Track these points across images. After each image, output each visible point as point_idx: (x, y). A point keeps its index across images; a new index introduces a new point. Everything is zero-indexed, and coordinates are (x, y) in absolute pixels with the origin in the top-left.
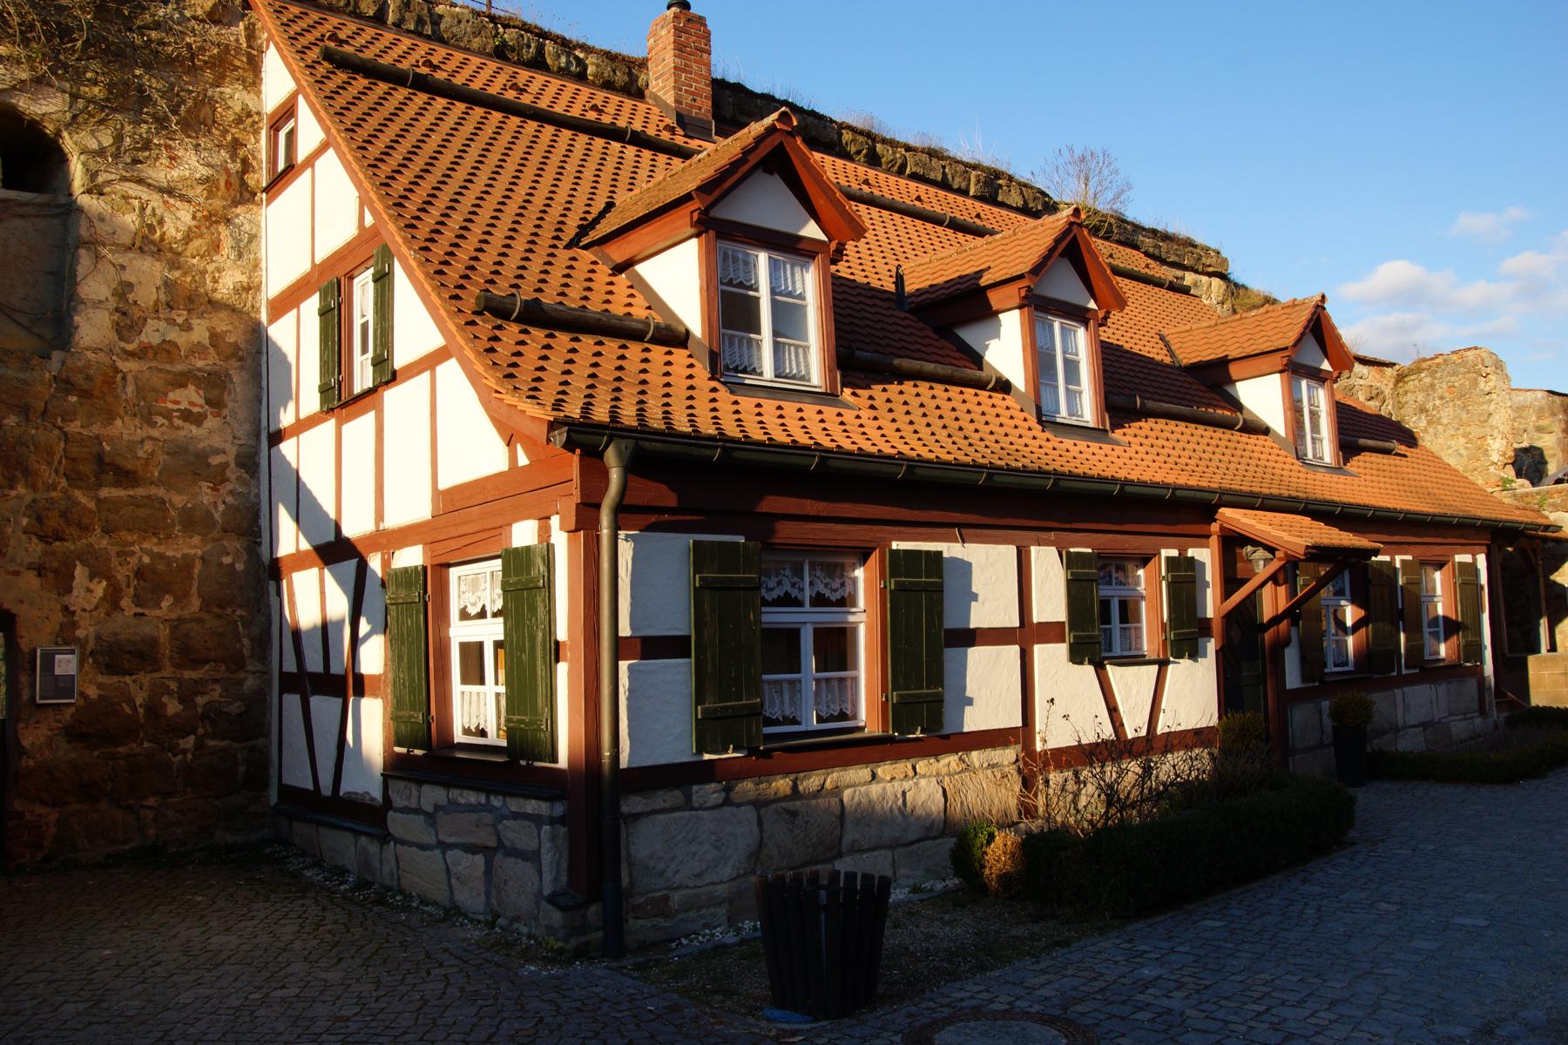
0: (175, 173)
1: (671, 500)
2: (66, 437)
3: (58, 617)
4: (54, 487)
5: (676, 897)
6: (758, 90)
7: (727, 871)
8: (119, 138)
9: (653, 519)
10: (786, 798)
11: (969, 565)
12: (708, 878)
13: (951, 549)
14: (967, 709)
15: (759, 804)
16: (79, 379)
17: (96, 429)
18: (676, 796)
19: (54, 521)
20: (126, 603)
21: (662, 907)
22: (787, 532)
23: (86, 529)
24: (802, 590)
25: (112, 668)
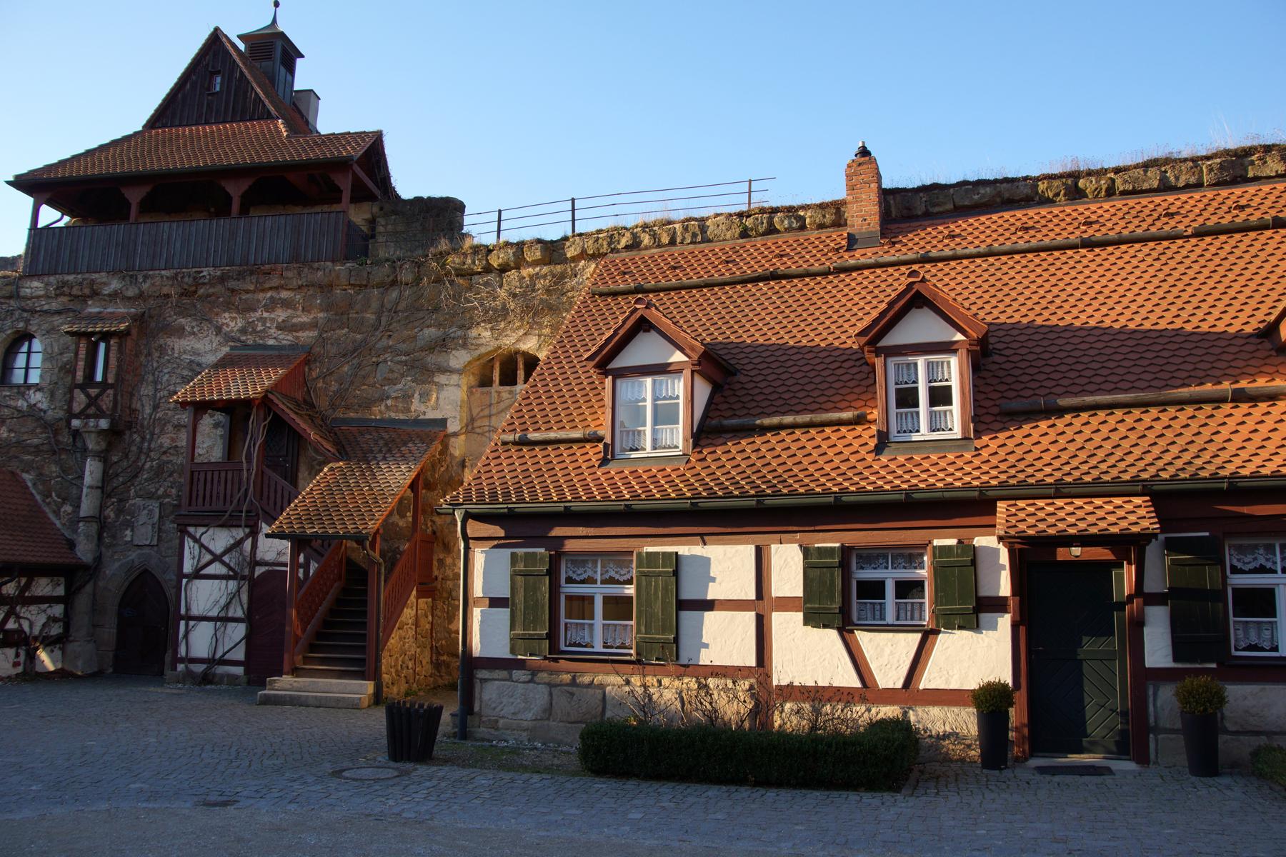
1: (502, 533)
5: (501, 722)
6: (953, 181)
7: (530, 716)
9: (496, 542)
10: (567, 685)
11: (708, 560)
13: (683, 550)
14: (703, 650)
15: (551, 685)
18: (504, 674)
21: (494, 725)
22: (570, 546)
24: (1275, 563)
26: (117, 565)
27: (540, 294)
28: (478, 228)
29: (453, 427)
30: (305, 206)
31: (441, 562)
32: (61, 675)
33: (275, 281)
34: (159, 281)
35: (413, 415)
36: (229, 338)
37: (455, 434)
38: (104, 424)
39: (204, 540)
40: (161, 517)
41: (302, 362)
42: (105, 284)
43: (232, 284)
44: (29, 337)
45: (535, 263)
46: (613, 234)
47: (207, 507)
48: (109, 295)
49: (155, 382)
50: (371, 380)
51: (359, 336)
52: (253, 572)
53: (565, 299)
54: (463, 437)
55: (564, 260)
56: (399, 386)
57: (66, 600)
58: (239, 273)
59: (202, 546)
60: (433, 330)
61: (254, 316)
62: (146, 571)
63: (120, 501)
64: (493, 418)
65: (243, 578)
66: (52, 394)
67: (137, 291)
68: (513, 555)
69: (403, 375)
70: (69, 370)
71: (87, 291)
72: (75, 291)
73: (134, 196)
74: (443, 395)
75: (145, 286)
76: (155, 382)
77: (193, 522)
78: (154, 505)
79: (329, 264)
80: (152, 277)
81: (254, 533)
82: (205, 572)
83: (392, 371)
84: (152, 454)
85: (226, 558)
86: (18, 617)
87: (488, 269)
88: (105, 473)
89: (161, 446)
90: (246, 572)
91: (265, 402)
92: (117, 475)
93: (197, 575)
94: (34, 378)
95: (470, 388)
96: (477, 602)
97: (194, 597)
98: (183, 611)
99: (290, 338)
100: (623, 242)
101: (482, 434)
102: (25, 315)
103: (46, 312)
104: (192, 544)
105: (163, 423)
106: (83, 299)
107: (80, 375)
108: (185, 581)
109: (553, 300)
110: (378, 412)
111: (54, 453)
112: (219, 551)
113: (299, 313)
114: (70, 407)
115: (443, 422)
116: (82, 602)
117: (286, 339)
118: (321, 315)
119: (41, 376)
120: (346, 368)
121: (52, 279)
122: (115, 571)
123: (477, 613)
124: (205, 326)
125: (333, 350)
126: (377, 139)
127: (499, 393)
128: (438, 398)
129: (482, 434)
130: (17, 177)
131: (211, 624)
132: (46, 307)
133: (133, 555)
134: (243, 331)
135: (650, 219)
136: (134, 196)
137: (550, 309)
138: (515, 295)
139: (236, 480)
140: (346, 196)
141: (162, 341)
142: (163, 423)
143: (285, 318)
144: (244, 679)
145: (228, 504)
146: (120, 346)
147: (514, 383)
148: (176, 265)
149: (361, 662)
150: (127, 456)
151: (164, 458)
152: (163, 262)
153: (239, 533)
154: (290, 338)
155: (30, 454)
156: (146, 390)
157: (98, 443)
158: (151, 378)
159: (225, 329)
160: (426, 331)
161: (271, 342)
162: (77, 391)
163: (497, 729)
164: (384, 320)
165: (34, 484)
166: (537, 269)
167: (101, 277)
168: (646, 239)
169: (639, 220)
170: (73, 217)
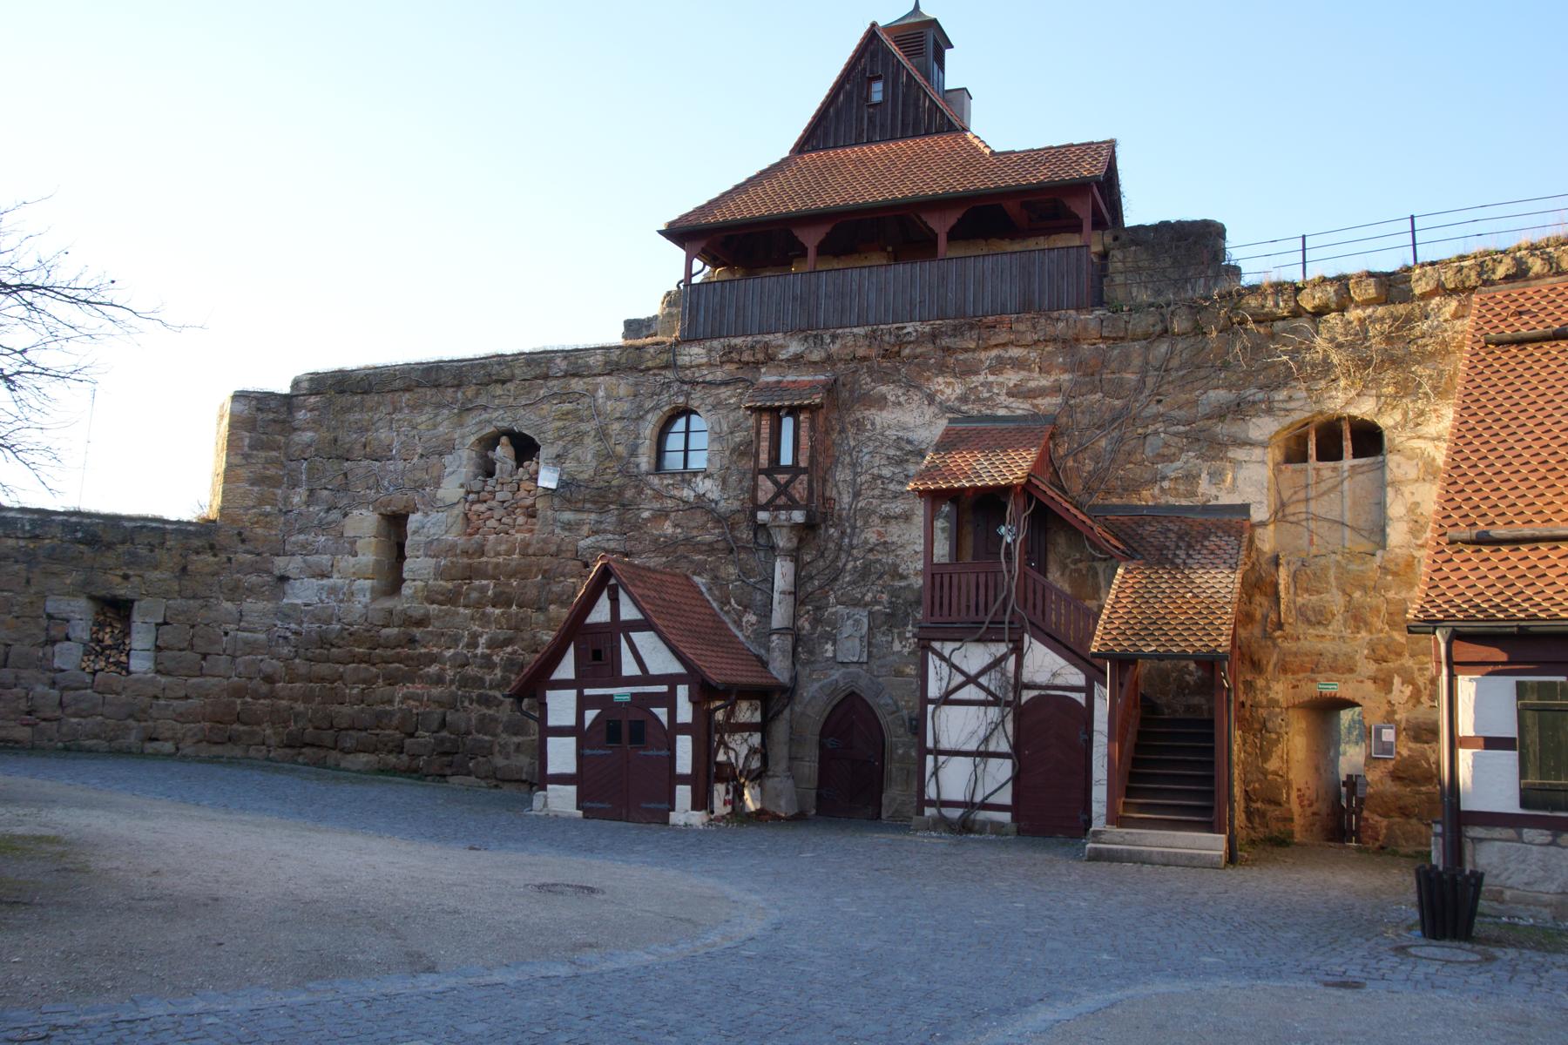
0: (1441, 426)
2: (1388, 601)
3: (1385, 707)
4: (1381, 631)
5: (1508, 894)
7: (1553, 888)
8: (1405, 414)
12: (1536, 888)
16: (1392, 567)
17: (1403, 595)
18: (1509, 833)
19: (1382, 652)
20: (1424, 699)
21: (1498, 897)
23: (1400, 655)
25: (1416, 738)
26: (816, 685)
27: (1376, 343)
28: (1257, 257)
29: (1259, 514)
30: (1012, 239)
31: (1249, 685)
32: (760, 816)
33: (1004, 337)
34: (851, 339)
35: (1197, 501)
36: (945, 408)
37: (1263, 524)
38: (798, 516)
39: (956, 660)
40: (870, 628)
41: (1046, 432)
42: (782, 347)
43: (946, 341)
44: (687, 412)
45: (1367, 303)
46: (1484, 262)
47: (954, 617)
48: (788, 360)
49: (854, 465)
50: (1138, 457)
51: (1118, 403)
52: (1018, 695)
53: (1413, 348)
54: (1271, 527)
55: (1407, 297)
56: (1178, 464)
57: (763, 728)
58: (955, 328)
59: (953, 666)
60: (1222, 392)
61: (976, 380)
62: (853, 693)
63: (817, 608)
64: (1312, 504)
65: (1008, 704)
66: (724, 481)
67: (823, 354)
68: (1518, 683)
69: (1182, 450)
70: (746, 450)
71: (760, 356)
72: (746, 357)
73: (811, 238)
74: (1243, 473)
75: (834, 348)
76: (854, 465)
77: (939, 635)
78: (862, 615)
79: (1072, 312)
80: (843, 336)
81: (1018, 651)
82: (953, 697)
83: (1167, 445)
84: (855, 552)
85: (983, 680)
86: (727, 747)
87: (1297, 312)
88: (797, 574)
89: (866, 542)
90: (1011, 697)
91: (1027, 490)
92: (812, 578)
93: (946, 700)
94: (698, 461)
95: (1277, 465)
96: (1467, 742)
97: (943, 727)
98: (930, 744)
99: (1027, 406)
100: (1501, 271)
101: (1297, 523)
102: (685, 387)
103: (710, 383)
104: (938, 662)
105: (867, 513)
106: (757, 365)
107: (764, 459)
108: (930, 708)
109: (1399, 350)
110: (1148, 497)
111: (731, 551)
112: (973, 671)
113: (1036, 375)
114: (754, 498)
115: (1244, 509)
116: (780, 730)
117: (1021, 407)
118: (1066, 377)
119: (709, 460)
120: (1103, 443)
121: (715, 343)
122: (815, 694)
123: (1465, 756)
124: (916, 396)
125: (1085, 421)
126: (1111, 145)
127: (1318, 470)
128: (1234, 479)
129: (1297, 523)
130: (671, 224)
131: (969, 760)
132: (709, 378)
133: (836, 674)
134: (963, 399)
135: (1537, 237)
136: (811, 238)
137: (1393, 362)
138: (1339, 346)
139: (991, 584)
140: (1087, 225)
141: (859, 415)
142: (867, 513)
143: (1016, 379)
144: (1013, 828)
145: (982, 613)
146: (812, 421)
147: (1338, 457)
148: (872, 320)
149: (1207, 810)
150: (822, 556)
151: (871, 556)
152: (854, 318)
153: (1002, 649)
154: (1027, 406)
155: (701, 553)
156: (842, 475)
157: (790, 540)
158: (848, 459)
159: (939, 397)
160: (1211, 393)
161: (1001, 412)
162: (762, 478)
163: (1502, 902)
164: (1150, 381)
165: (710, 589)
166: (1369, 311)
167: (777, 338)
168: (1537, 265)
169: (1525, 238)
170: (715, 266)
